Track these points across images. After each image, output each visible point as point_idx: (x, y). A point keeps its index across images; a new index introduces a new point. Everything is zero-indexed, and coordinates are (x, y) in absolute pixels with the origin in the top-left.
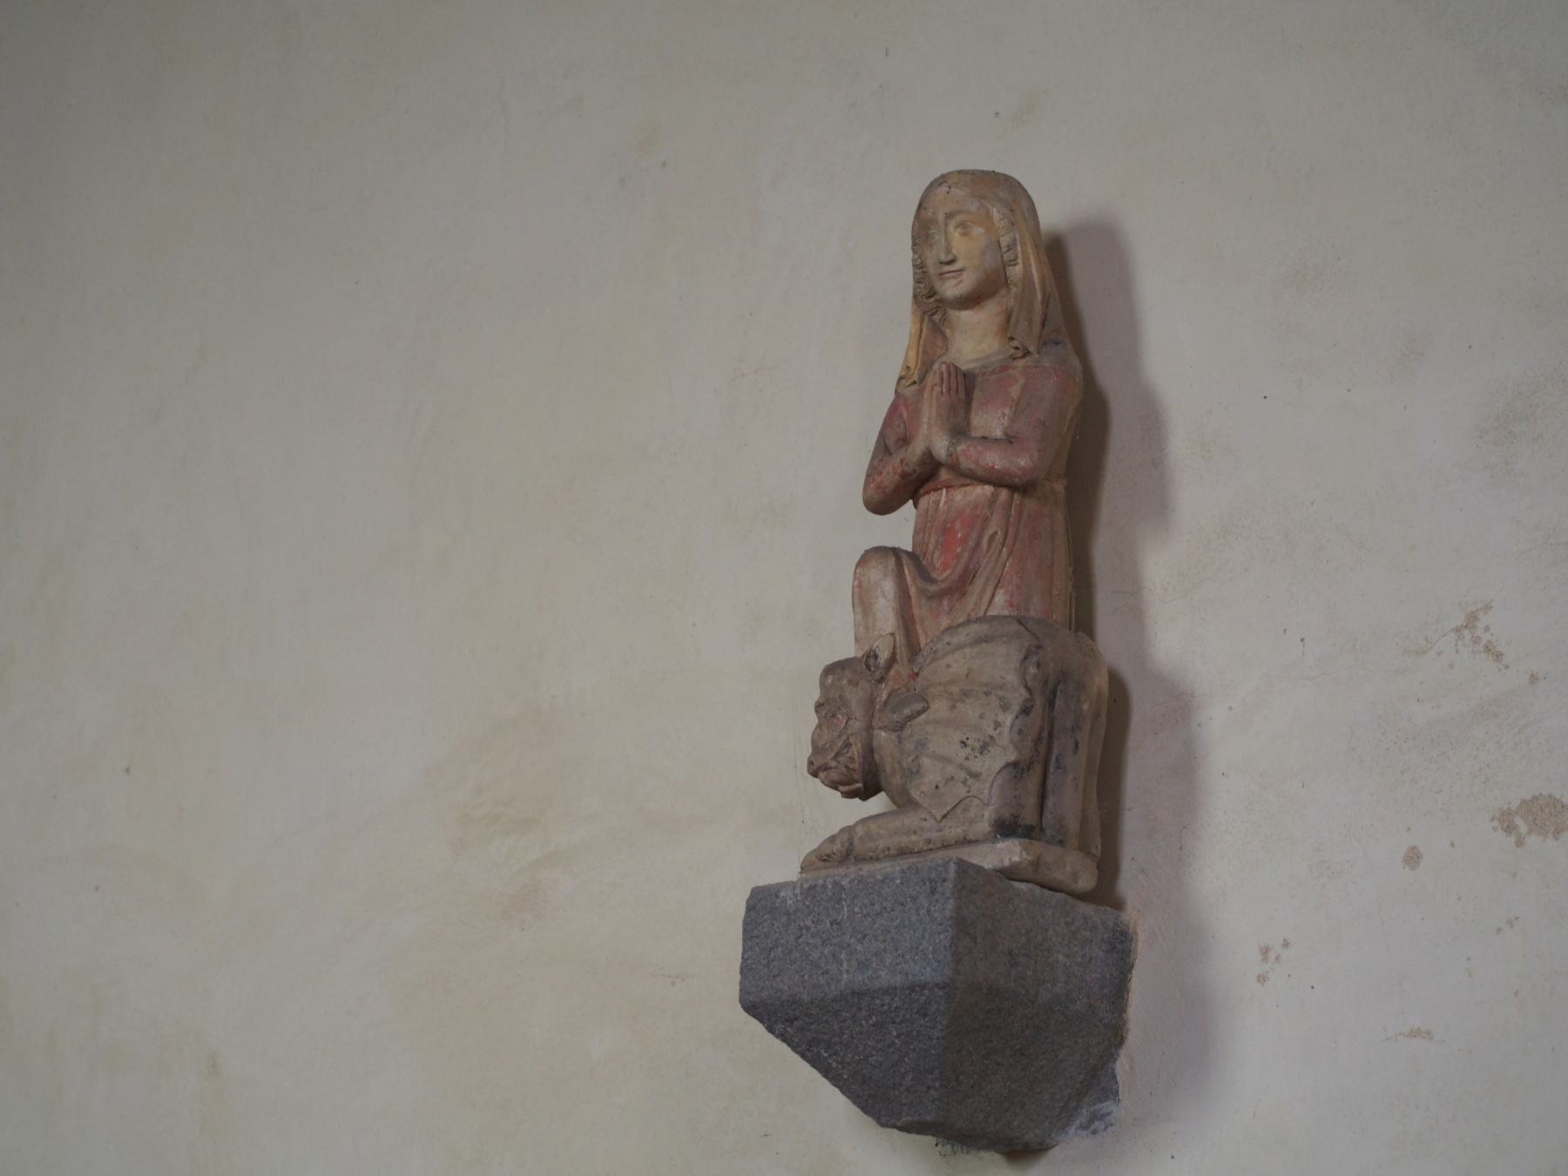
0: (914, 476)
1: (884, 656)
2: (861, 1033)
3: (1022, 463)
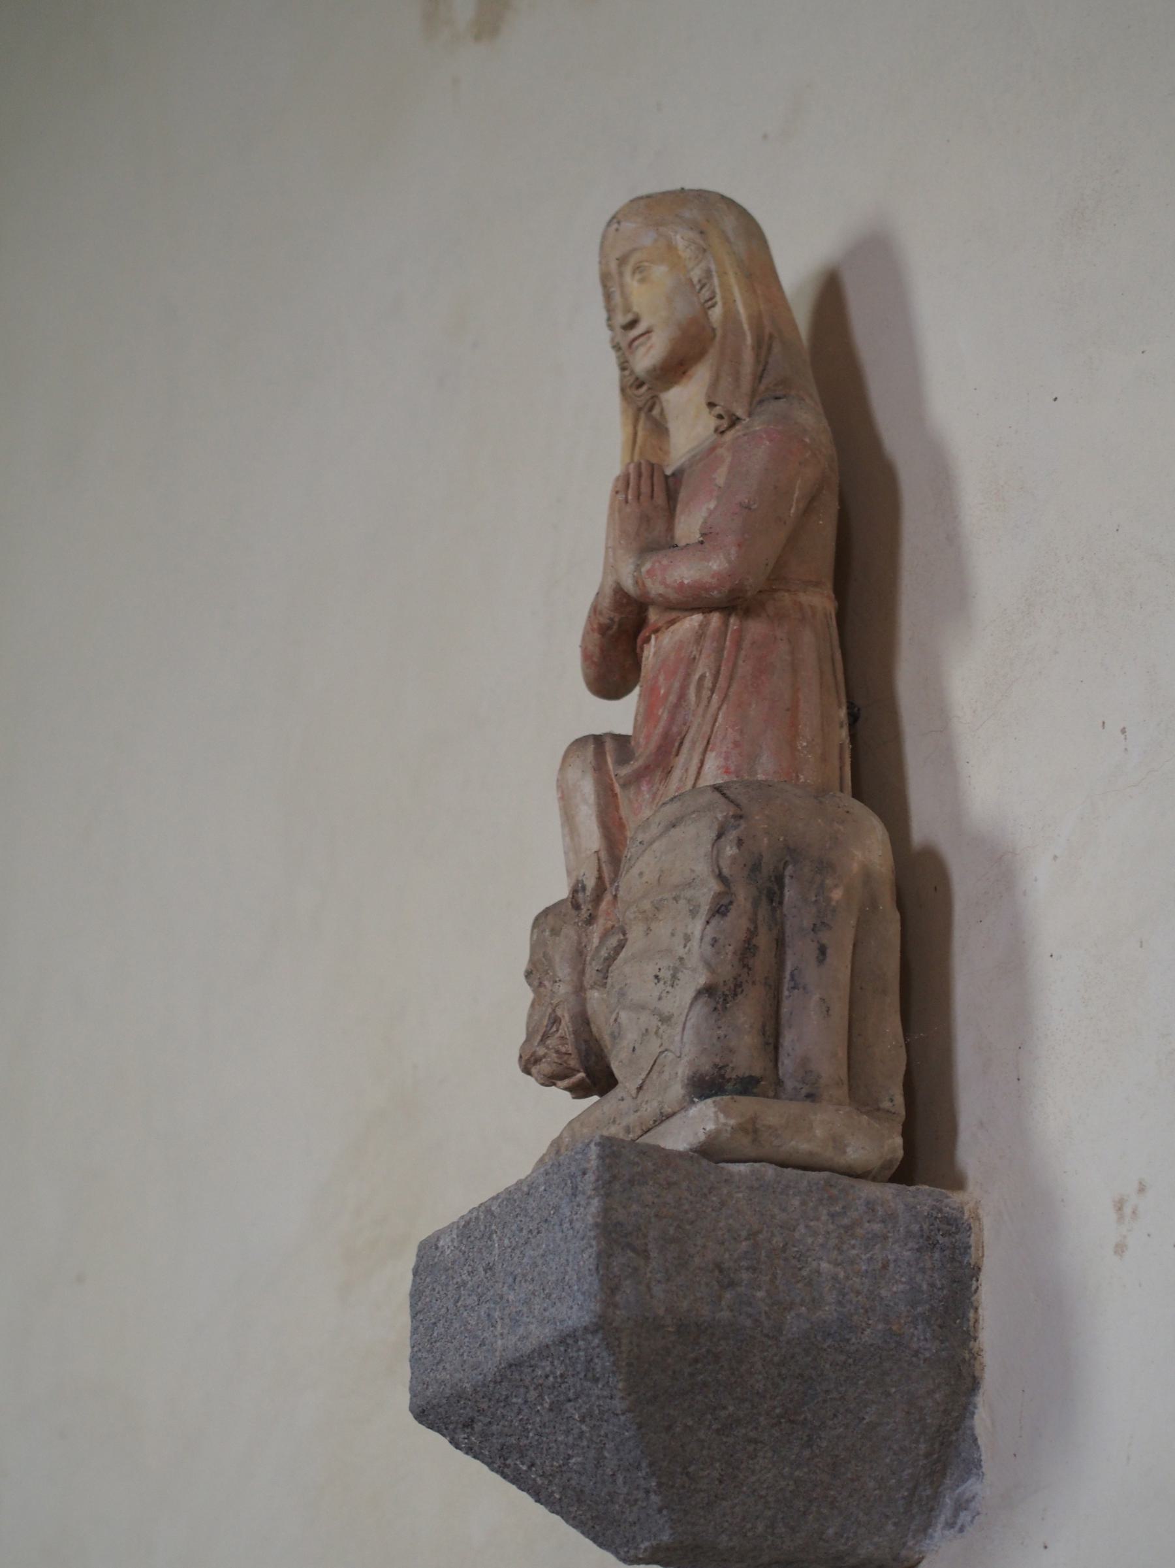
0: (615, 627)
1: (591, 883)
2: (544, 1425)
3: (715, 567)
